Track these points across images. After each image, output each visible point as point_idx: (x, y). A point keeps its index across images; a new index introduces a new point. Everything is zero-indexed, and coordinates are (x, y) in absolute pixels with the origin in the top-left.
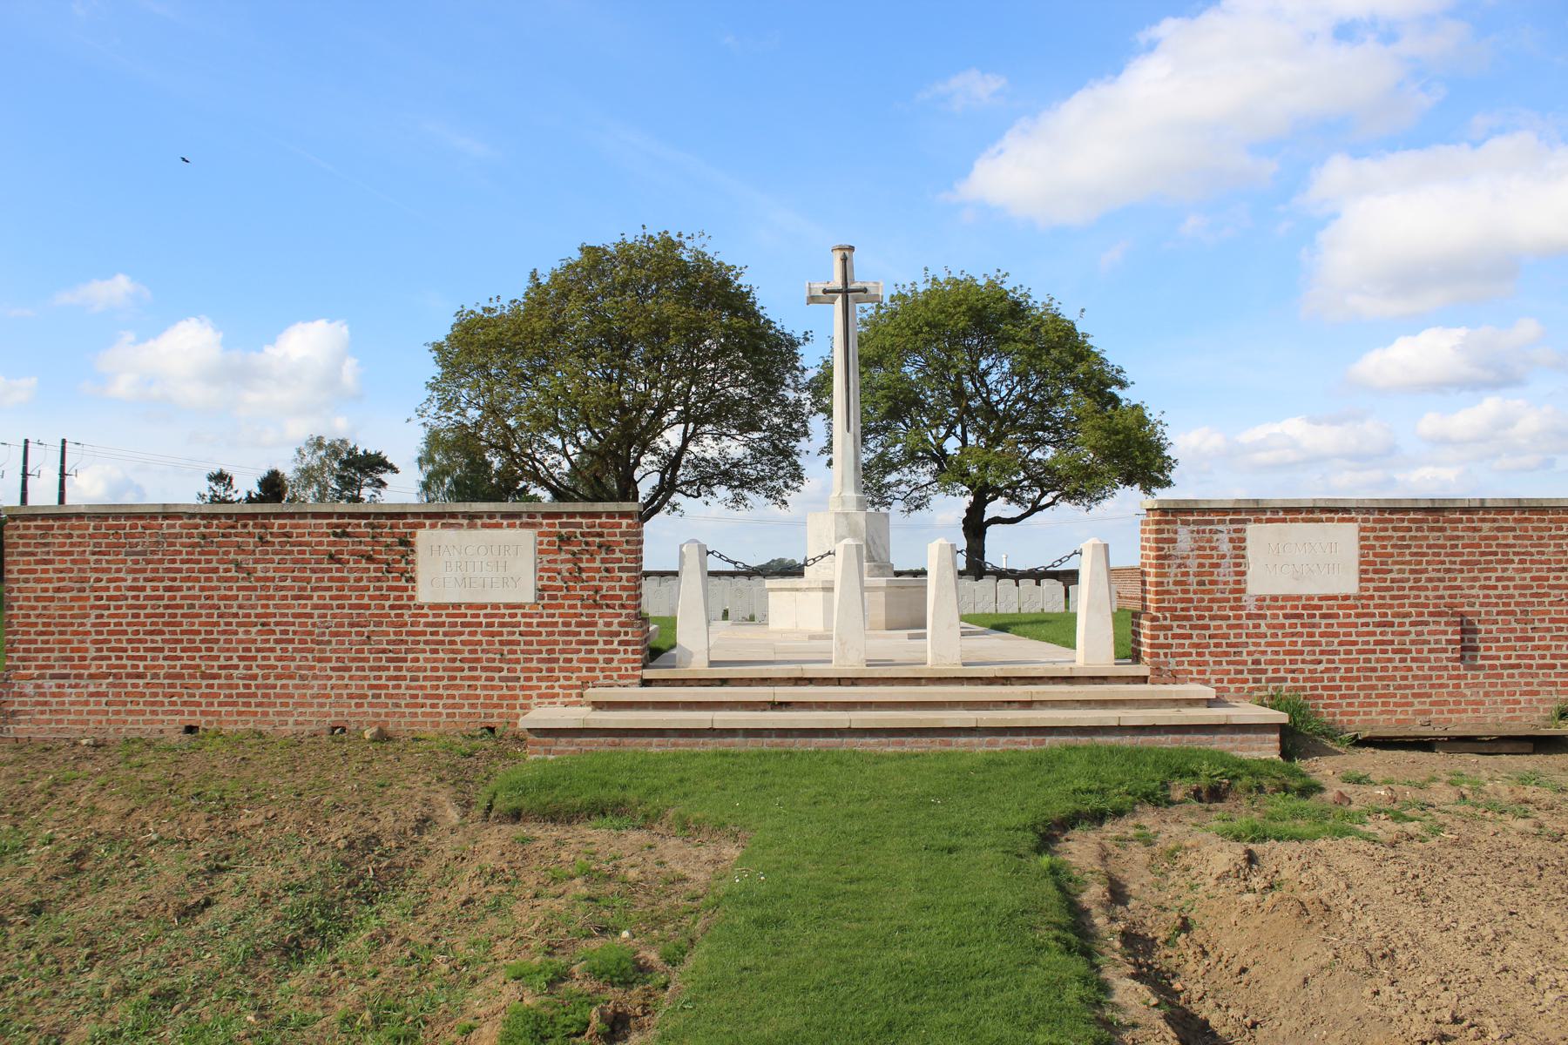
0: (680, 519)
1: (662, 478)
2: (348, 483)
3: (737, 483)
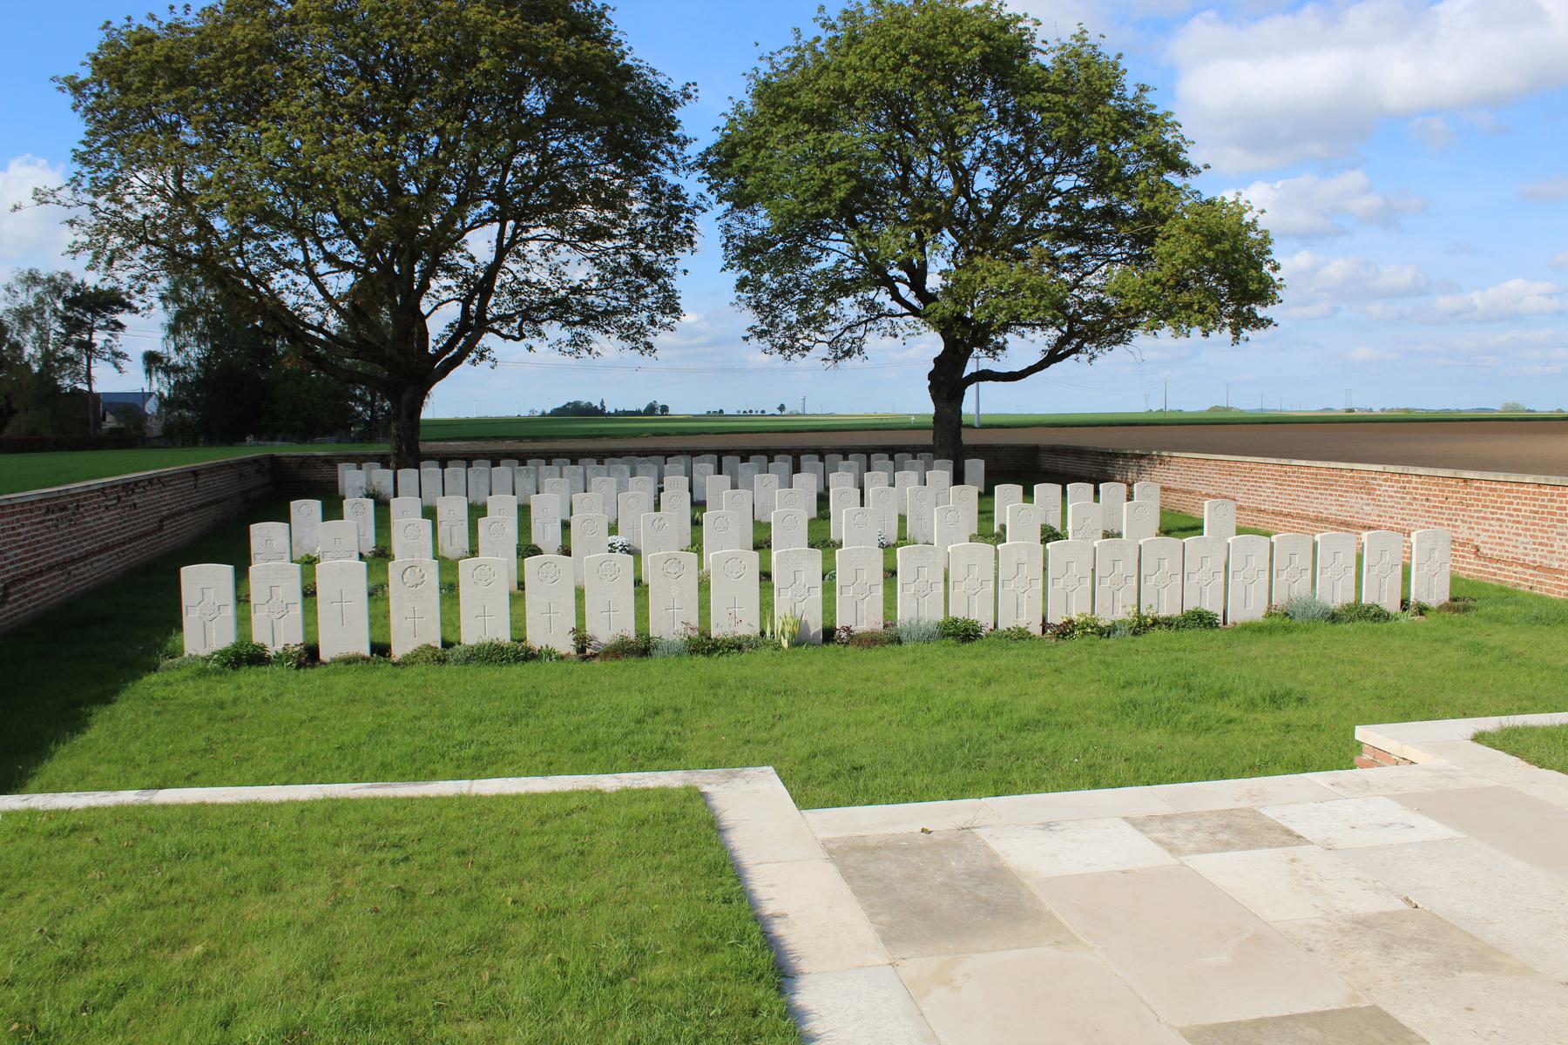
0: (489, 368)
1: (465, 311)
2: (73, 326)
3: (577, 318)
